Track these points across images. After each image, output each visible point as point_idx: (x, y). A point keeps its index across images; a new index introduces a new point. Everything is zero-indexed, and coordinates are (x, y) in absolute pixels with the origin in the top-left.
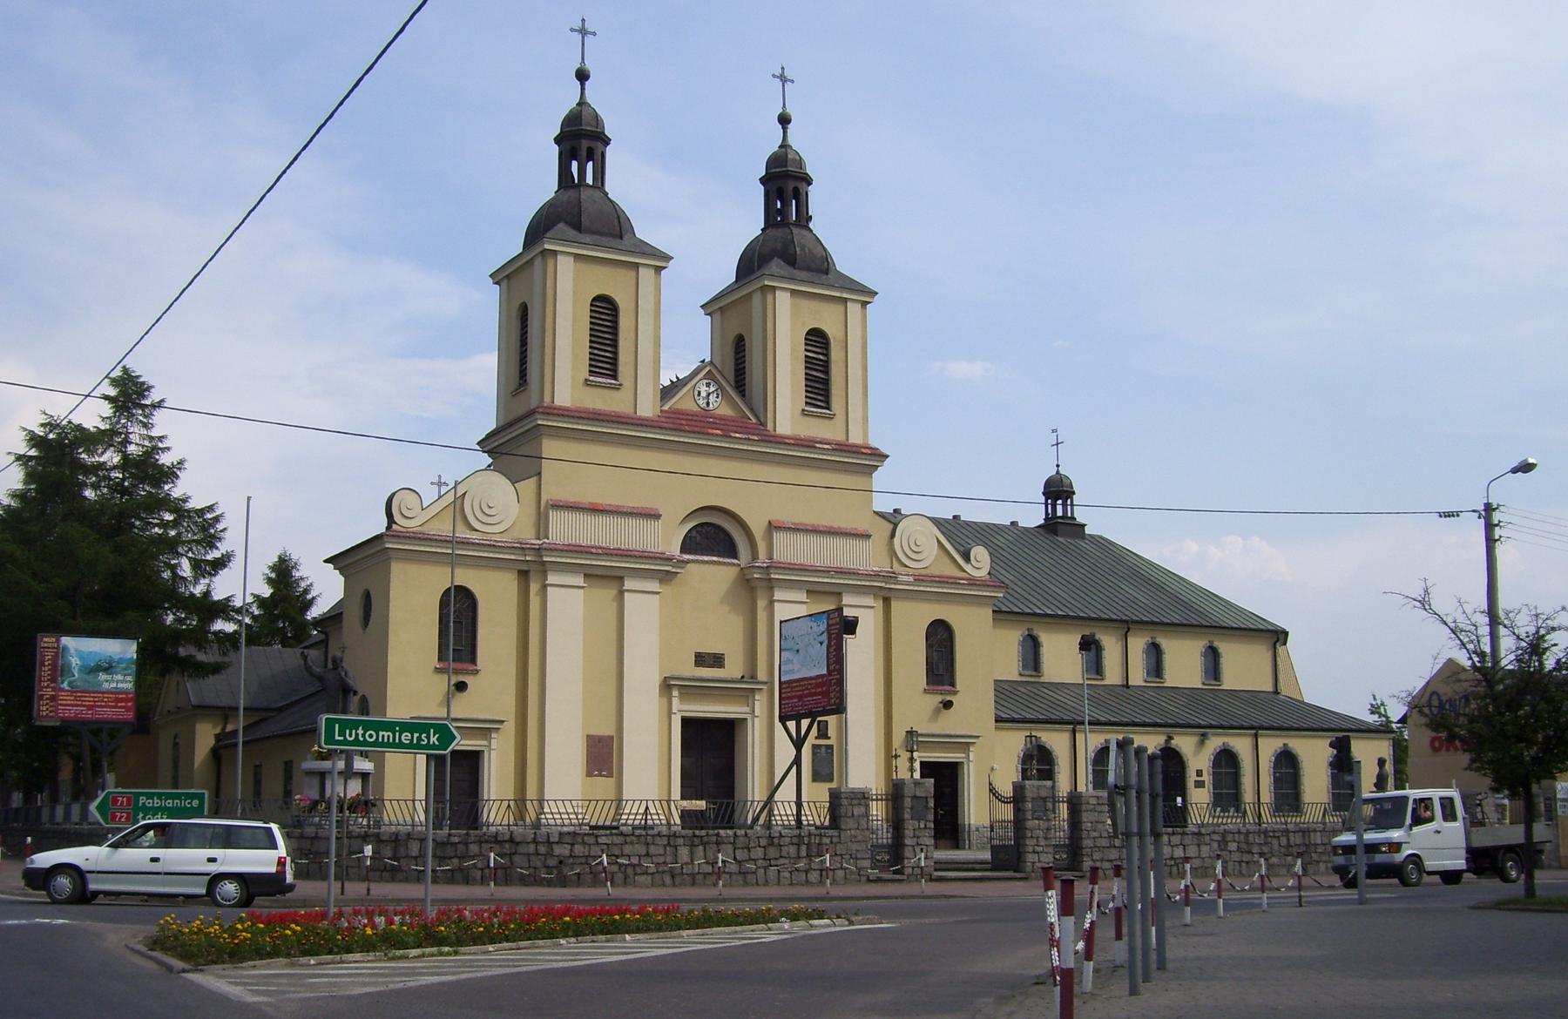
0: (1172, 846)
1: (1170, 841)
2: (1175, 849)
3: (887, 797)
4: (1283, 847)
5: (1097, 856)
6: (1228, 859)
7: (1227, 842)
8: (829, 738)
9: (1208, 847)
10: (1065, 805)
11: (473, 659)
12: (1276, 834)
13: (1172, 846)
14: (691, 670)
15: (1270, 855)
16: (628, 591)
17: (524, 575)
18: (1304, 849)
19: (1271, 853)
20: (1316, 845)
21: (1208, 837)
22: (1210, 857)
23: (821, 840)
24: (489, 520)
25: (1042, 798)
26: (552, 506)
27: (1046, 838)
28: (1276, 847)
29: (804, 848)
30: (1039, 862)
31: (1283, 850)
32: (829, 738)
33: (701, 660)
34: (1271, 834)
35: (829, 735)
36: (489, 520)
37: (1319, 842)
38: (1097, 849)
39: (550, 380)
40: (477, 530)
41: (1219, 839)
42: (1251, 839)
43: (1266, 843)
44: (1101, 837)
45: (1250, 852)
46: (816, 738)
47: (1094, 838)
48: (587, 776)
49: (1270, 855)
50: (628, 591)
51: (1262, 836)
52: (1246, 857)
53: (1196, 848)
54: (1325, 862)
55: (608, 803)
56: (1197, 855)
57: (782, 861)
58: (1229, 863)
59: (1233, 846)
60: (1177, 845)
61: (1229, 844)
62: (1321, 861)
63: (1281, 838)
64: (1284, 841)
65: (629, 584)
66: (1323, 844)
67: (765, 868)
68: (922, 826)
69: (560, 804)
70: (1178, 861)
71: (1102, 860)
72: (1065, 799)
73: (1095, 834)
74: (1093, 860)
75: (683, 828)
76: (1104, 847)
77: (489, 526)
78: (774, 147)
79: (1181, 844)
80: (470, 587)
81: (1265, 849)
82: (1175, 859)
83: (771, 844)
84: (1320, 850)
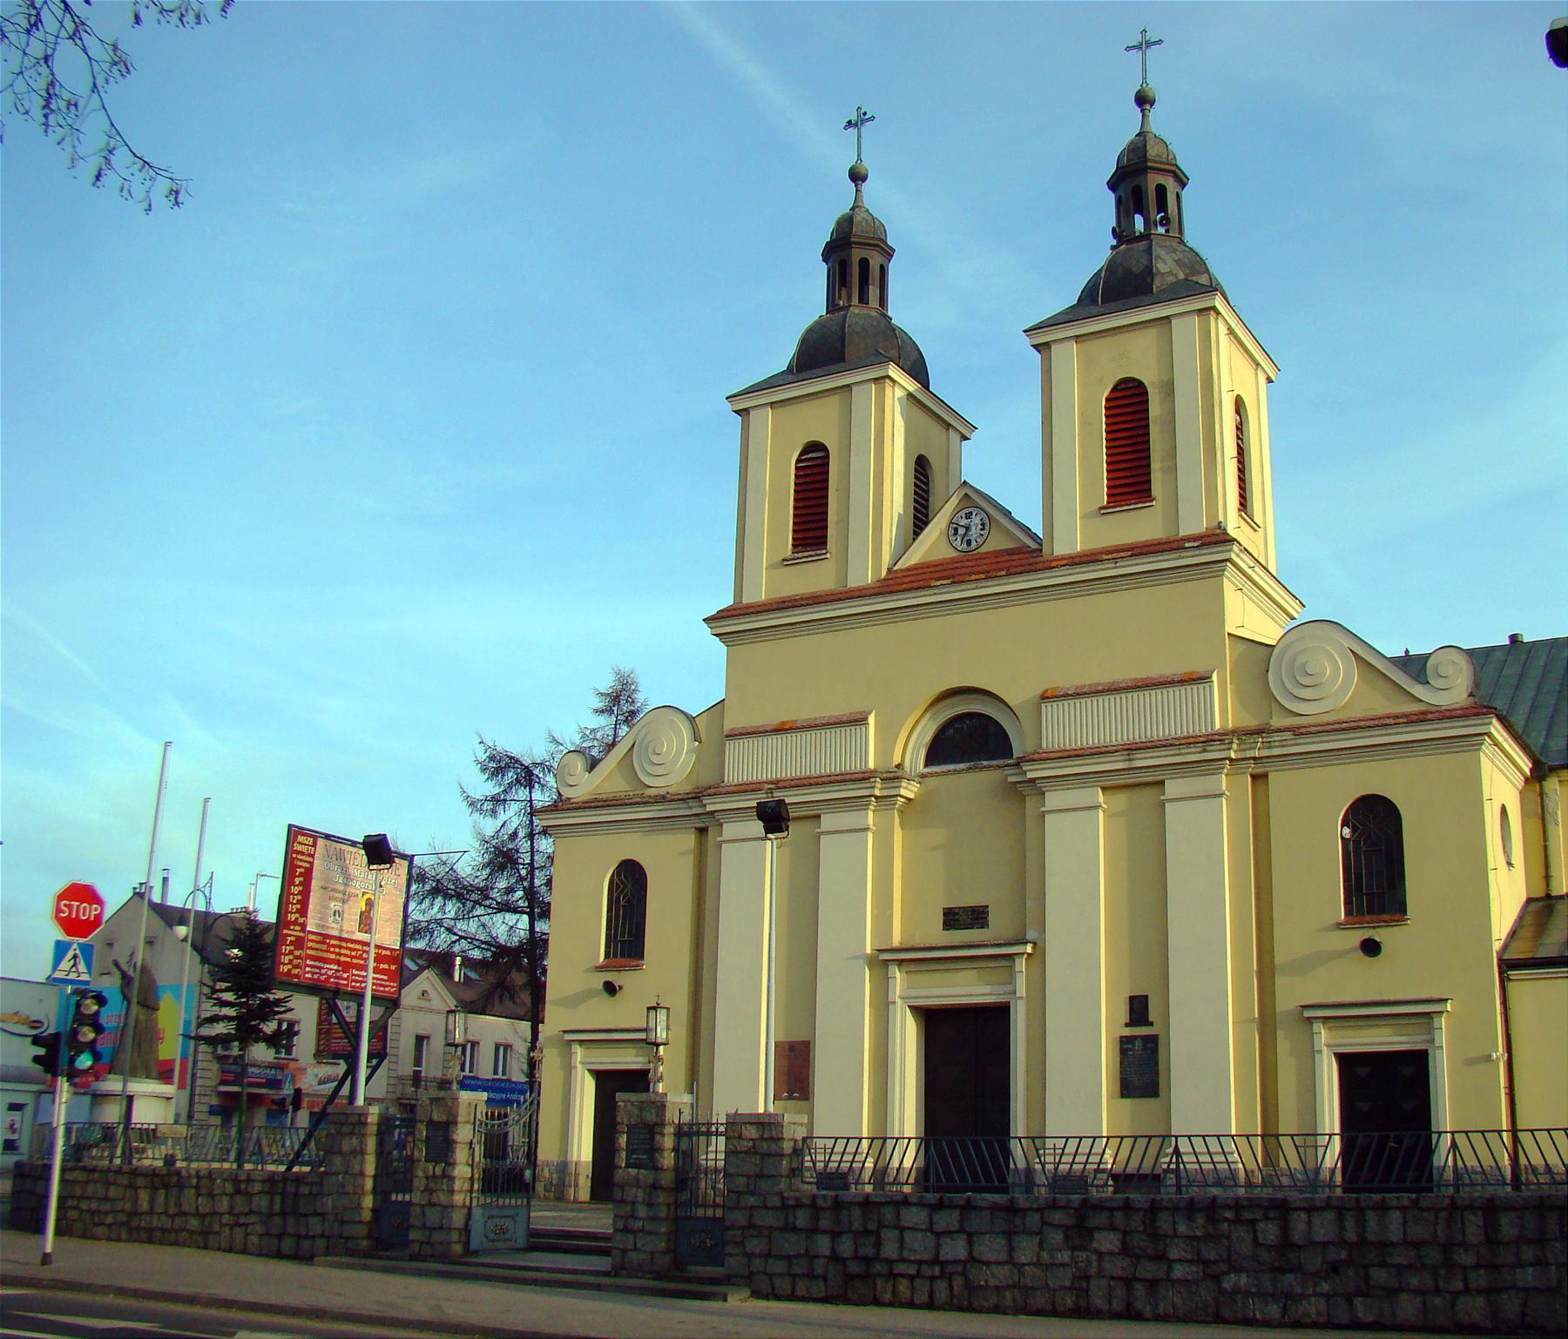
0: (938, 1234)
1: (931, 1222)
2: (946, 1240)
3: (108, 1133)
4: (1269, 1247)
5: (755, 1245)
6: (1093, 1271)
7: (1091, 1230)
8: (1151, 1024)
9: (1037, 1239)
10: (722, 1139)
11: (639, 954)
12: (1246, 1215)
13: (938, 1234)
14: (935, 933)
15: (1224, 1267)
16: (1170, 800)
17: (702, 831)
18: (1343, 1255)
19: (1229, 1260)
20: (1384, 1246)
21: (1037, 1216)
22: (1038, 1264)
23: (297, 1188)
24: (1305, 693)
25: (646, 1125)
26: (727, 736)
27: (650, 1205)
28: (1245, 1248)
29: (277, 1199)
30: (635, 1249)
31: (1264, 1255)
32: (1151, 1024)
33: (952, 918)
34: (1229, 1214)
35: (1150, 1020)
36: (1305, 693)
37: (1395, 1234)
38: (755, 1232)
39: (1260, 489)
40: (1421, 701)
41: (1070, 1221)
42: (1164, 1223)
43: (1210, 1237)
44: (765, 1207)
45: (1161, 1257)
46: (1127, 1025)
47: (752, 1208)
48: (1123, 1096)
49: (1224, 1267)
50: (1170, 800)
51: (1200, 1220)
52: (1148, 1270)
53: (1000, 1242)
54: (1417, 1292)
55: (1142, 1142)
56: (1003, 1256)
57: (253, 1218)
58: (1094, 1283)
59: (1107, 1241)
60: (950, 1232)
61: (1097, 1235)
62: (1401, 1290)
63: (1261, 1226)
64: (1269, 1232)
65: (1173, 787)
66: (198, 1214)
67: (232, 1227)
68: (438, 1171)
69: (1213, 1142)
70: (950, 1269)
71: (767, 1255)
72: (722, 1129)
73: (752, 1200)
74: (746, 1254)
75: (1345, 1191)
76: (770, 1228)
77: (1307, 704)
78: (845, 209)
79: (961, 1231)
80: (1363, 794)
81: (1210, 1253)
82: (943, 1264)
83: (238, 1192)
84: (1398, 1260)
